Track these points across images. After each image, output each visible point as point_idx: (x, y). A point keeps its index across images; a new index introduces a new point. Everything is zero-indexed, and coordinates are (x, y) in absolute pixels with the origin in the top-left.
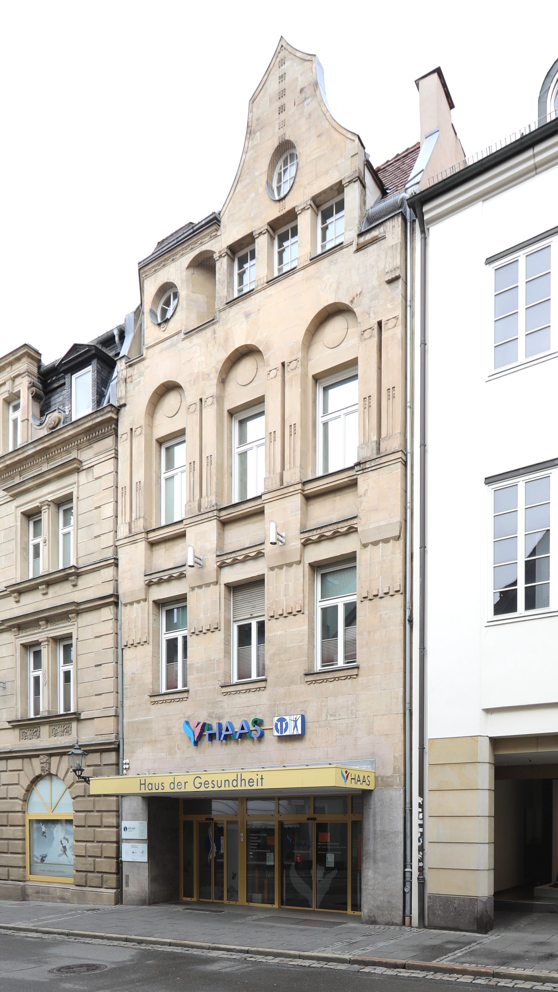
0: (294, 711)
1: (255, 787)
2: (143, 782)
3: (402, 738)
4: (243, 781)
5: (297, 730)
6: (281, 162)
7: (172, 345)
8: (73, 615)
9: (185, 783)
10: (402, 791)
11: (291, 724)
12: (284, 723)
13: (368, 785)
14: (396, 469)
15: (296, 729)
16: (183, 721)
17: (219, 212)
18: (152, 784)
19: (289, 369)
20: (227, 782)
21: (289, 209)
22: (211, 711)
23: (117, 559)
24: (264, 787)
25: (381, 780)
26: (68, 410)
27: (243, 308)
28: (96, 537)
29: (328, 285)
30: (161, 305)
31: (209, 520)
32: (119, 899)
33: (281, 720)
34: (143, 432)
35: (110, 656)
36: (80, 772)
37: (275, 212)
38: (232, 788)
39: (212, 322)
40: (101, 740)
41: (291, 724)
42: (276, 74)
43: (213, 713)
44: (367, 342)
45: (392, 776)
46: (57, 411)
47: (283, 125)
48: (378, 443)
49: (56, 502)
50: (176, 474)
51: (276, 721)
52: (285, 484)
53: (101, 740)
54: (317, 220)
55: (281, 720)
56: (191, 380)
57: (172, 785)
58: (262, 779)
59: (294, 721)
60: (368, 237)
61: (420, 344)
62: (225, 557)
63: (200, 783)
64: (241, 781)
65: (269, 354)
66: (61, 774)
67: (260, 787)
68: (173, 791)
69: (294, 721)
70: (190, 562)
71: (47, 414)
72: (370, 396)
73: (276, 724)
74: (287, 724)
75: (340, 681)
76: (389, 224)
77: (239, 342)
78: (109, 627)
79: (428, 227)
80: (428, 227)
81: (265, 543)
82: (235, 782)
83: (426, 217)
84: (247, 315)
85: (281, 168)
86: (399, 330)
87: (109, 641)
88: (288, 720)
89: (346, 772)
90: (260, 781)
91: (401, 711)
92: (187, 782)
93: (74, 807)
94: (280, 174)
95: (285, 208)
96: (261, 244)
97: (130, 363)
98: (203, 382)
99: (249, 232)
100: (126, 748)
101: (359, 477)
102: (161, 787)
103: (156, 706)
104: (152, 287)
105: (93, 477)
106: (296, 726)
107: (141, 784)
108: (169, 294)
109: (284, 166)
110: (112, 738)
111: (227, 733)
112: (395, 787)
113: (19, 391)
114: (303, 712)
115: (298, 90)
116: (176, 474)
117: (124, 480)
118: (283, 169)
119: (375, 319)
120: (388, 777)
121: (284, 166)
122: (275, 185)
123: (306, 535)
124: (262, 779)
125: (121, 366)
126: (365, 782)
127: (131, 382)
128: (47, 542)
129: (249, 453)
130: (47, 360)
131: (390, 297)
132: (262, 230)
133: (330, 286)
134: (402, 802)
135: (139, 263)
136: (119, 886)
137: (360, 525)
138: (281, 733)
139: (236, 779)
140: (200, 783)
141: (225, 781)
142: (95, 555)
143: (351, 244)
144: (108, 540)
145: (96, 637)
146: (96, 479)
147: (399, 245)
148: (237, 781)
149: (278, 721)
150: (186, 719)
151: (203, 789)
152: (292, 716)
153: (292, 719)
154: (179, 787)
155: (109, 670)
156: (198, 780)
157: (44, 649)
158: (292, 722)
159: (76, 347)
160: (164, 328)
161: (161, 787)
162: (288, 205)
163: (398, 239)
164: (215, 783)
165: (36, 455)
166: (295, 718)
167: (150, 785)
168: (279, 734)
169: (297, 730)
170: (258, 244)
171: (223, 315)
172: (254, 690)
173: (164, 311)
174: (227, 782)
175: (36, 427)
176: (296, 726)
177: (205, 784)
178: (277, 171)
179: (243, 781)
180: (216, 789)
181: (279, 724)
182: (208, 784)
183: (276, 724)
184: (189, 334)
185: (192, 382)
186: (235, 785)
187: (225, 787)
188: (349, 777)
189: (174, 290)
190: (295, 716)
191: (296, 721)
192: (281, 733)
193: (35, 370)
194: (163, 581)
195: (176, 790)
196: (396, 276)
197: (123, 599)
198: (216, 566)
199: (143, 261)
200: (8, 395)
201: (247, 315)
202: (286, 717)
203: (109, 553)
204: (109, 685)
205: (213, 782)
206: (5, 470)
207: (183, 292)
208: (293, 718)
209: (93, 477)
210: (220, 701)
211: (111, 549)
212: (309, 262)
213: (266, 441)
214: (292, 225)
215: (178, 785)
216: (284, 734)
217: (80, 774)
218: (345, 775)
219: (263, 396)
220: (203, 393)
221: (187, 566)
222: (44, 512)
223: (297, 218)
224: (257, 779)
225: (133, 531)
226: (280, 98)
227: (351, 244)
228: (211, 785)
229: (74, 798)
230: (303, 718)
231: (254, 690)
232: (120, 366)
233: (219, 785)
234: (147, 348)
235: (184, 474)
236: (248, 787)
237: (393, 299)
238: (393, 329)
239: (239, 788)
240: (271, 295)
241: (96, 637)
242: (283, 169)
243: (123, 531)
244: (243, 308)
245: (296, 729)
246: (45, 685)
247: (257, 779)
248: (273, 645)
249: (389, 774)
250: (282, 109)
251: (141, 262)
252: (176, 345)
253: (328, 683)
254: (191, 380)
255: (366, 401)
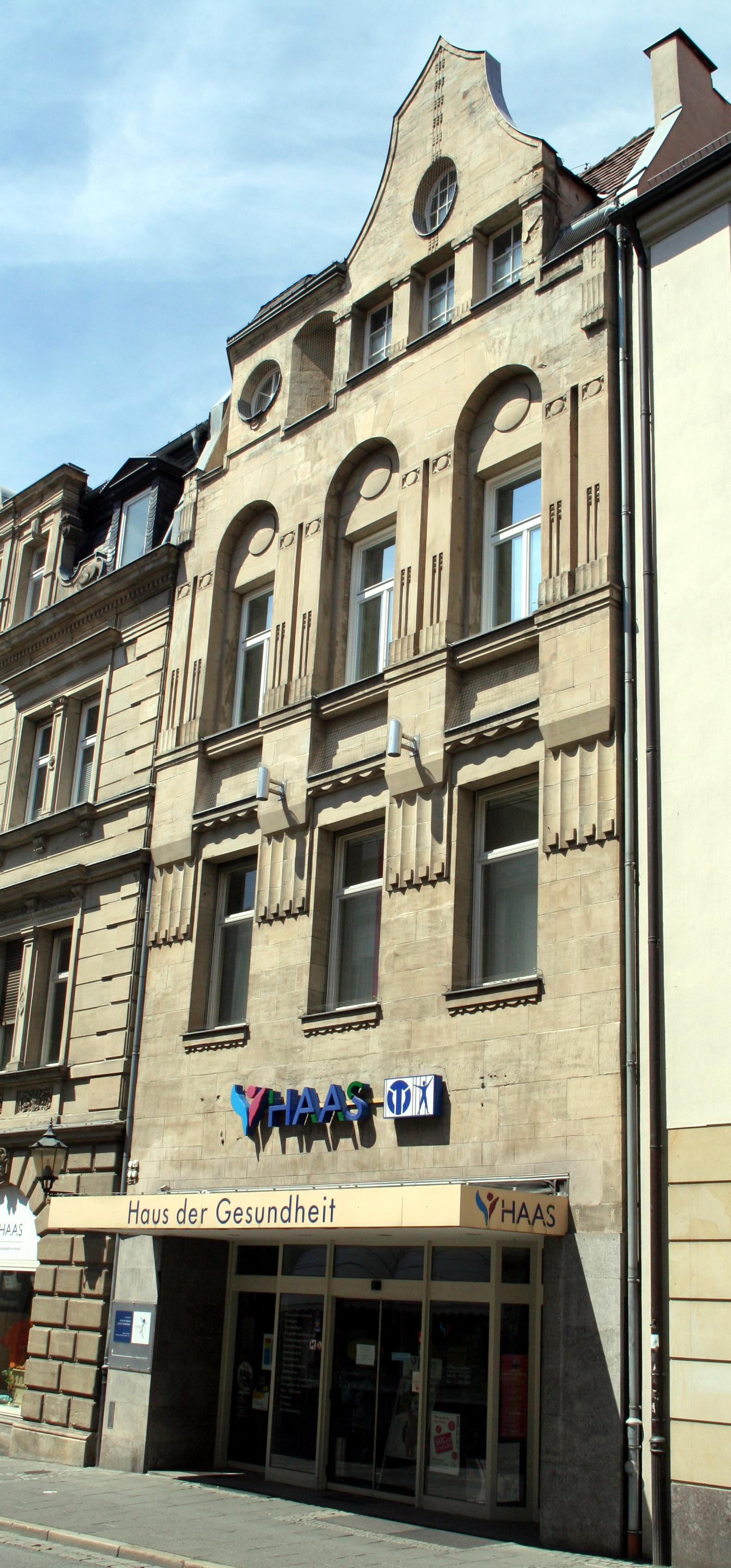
0: (425, 1067)
1: (319, 1224)
2: (134, 1207)
3: (619, 1127)
4: (300, 1211)
5: (426, 1106)
6: (437, 184)
7: (266, 448)
8: (78, 888)
9: (203, 1211)
10: (618, 1242)
11: (417, 1094)
12: (403, 1092)
13: (551, 1226)
14: (603, 617)
15: (424, 1103)
16: (231, 1085)
17: (343, 261)
18: (148, 1212)
19: (436, 470)
20: (273, 1211)
21: (443, 245)
22: (283, 1066)
23: (152, 790)
24: (204, 1226)
25: (580, 1214)
26: (111, 555)
27: (371, 385)
28: (128, 753)
29: (497, 342)
30: (258, 392)
31: (299, 718)
32: (91, 1458)
33: (399, 1086)
34: (213, 581)
35: (125, 961)
36: (49, 1182)
37: (422, 250)
38: (280, 1224)
39: (325, 412)
40: (96, 1120)
41: (417, 1094)
42: (432, 77)
43: (285, 1070)
44: (555, 419)
45: (600, 1207)
46: (96, 558)
47: (438, 141)
48: (572, 576)
49: (78, 698)
50: (519, 535)
51: (388, 1088)
52: (423, 652)
53: (96, 1120)
54: (486, 253)
55: (399, 1086)
56: (289, 497)
57: (181, 1214)
58: (332, 1207)
59: (420, 1087)
60: (557, 273)
61: (640, 414)
62: (484, 728)
63: (227, 1212)
64: (297, 1209)
65: (406, 449)
66: (25, 1188)
67: (328, 1224)
68: (183, 1226)
69: (420, 1087)
70: (390, 750)
71: (81, 564)
72: (560, 502)
73: (390, 1094)
74: (408, 1094)
75: (507, 1008)
76: (587, 250)
77: (363, 435)
78: (129, 909)
79: (648, 246)
80: (648, 246)
81: (541, 703)
82: (286, 1211)
83: (642, 235)
84: (377, 396)
85: (437, 192)
86: (604, 398)
87: (127, 934)
88: (410, 1087)
89: (490, 1196)
90: (328, 1210)
91: (617, 1069)
92: (206, 1209)
93: (39, 1252)
94: (435, 200)
95: (437, 245)
96: (402, 298)
97: (204, 480)
98: (306, 500)
99: (386, 281)
100: (137, 1136)
101: (540, 634)
102: (163, 1218)
103: (194, 1056)
104: (246, 368)
105: (134, 655)
106: (424, 1098)
107: (131, 1211)
108: (270, 376)
109: (441, 189)
110: (113, 1118)
111: (305, 1110)
112: (606, 1231)
113: (48, 532)
114: (439, 1070)
115: (461, 95)
116: (519, 535)
117: (176, 662)
118: (439, 193)
119: (568, 383)
120: (592, 1208)
121: (441, 189)
122: (427, 215)
123: (317, 783)
124: (332, 1207)
125: (190, 485)
126: (542, 1218)
127: (203, 507)
128: (55, 765)
129: (516, 544)
130: (94, 483)
131: (590, 351)
132: (403, 277)
133: (501, 343)
134: (617, 1265)
135: (229, 340)
136: (96, 1427)
137: (544, 717)
138: (398, 1112)
139: (288, 1206)
140: (227, 1212)
141: (270, 1209)
142: (122, 782)
143: (531, 282)
144: (144, 758)
145: (110, 927)
146: (139, 658)
147: (602, 276)
148: (290, 1210)
149: (393, 1087)
150: (238, 1083)
151: (231, 1224)
152: (418, 1078)
153: (418, 1084)
154: (193, 1219)
155: (122, 988)
156: (225, 1206)
157: (28, 948)
158: (418, 1089)
159: (132, 463)
160: (256, 427)
161: (163, 1218)
162: (443, 238)
163: (601, 267)
164: (252, 1212)
165: (55, 626)
166: (424, 1083)
167: (145, 1213)
168: (395, 1115)
169: (426, 1106)
170: (397, 296)
171: (342, 399)
172: (340, 1029)
173: (262, 399)
174: (273, 1211)
175: (63, 583)
176: (424, 1098)
177: (235, 1214)
178: (431, 196)
179: (300, 1211)
180: (254, 1224)
181: (395, 1093)
182: (241, 1214)
183: (390, 1094)
184: (291, 432)
185: (291, 499)
186: (285, 1217)
187: (269, 1222)
188: (498, 1207)
189: (274, 371)
190: (423, 1079)
191: (424, 1089)
192: (398, 1112)
193: (75, 497)
194: (341, 788)
195: (187, 1225)
196: (598, 321)
197: (159, 859)
198: (305, 797)
199: (234, 336)
200: (32, 539)
201: (377, 396)
202: (409, 1081)
203: (143, 780)
204: (119, 1016)
205: (250, 1211)
206: (10, 652)
207: (286, 373)
208: (419, 1081)
209: (134, 655)
210: (299, 1047)
211: (148, 773)
212: (469, 313)
213: (395, 584)
214: (447, 265)
215: (190, 1215)
216: (403, 1115)
217: (49, 1187)
218: (488, 1204)
219: (272, 574)
220: (305, 515)
221: (387, 756)
222: (57, 716)
223: (392, 295)
224: (325, 1207)
225: (183, 740)
226: (435, 108)
227: (531, 282)
228: (245, 1217)
229: (41, 1235)
230: (439, 1081)
231: (340, 1029)
232: (190, 485)
233: (259, 1218)
234: (230, 457)
235: (538, 535)
236: (307, 1224)
237: (595, 352)
238: (595, 397)
239: (292, 1224)
240: (413, 363)
241: (110, 927)
242: (439, 193)
243: (167, 742)
244: (371, 385)
245: (424, 1103)
246: (21, 1014)
247: (325, 1207)
248: (394, 939)
249: (596, 1202)
250: (438, 121)
251: (231, 338)
252: (270, 448)
253: (467, 1015)
254: (289, 497)
255: (553, 509)
